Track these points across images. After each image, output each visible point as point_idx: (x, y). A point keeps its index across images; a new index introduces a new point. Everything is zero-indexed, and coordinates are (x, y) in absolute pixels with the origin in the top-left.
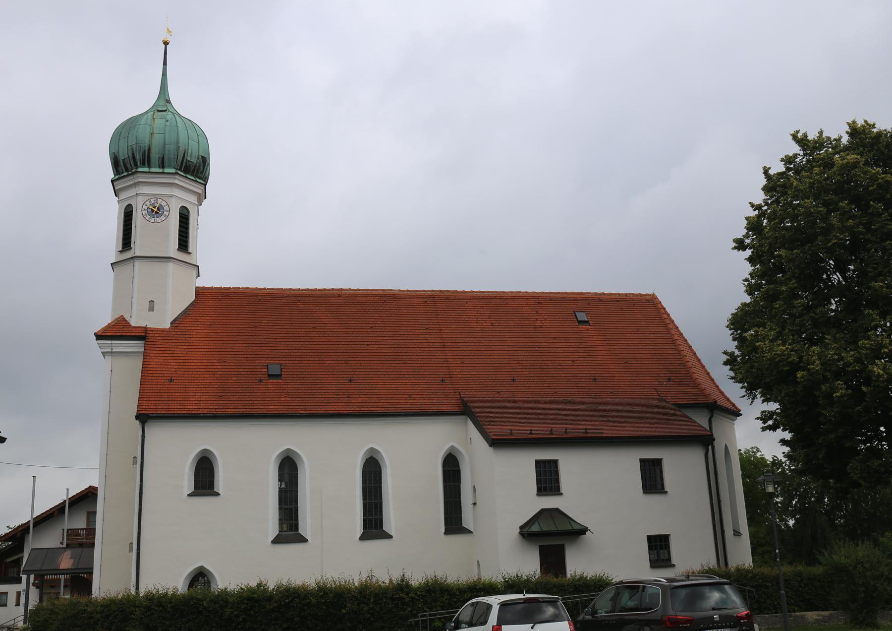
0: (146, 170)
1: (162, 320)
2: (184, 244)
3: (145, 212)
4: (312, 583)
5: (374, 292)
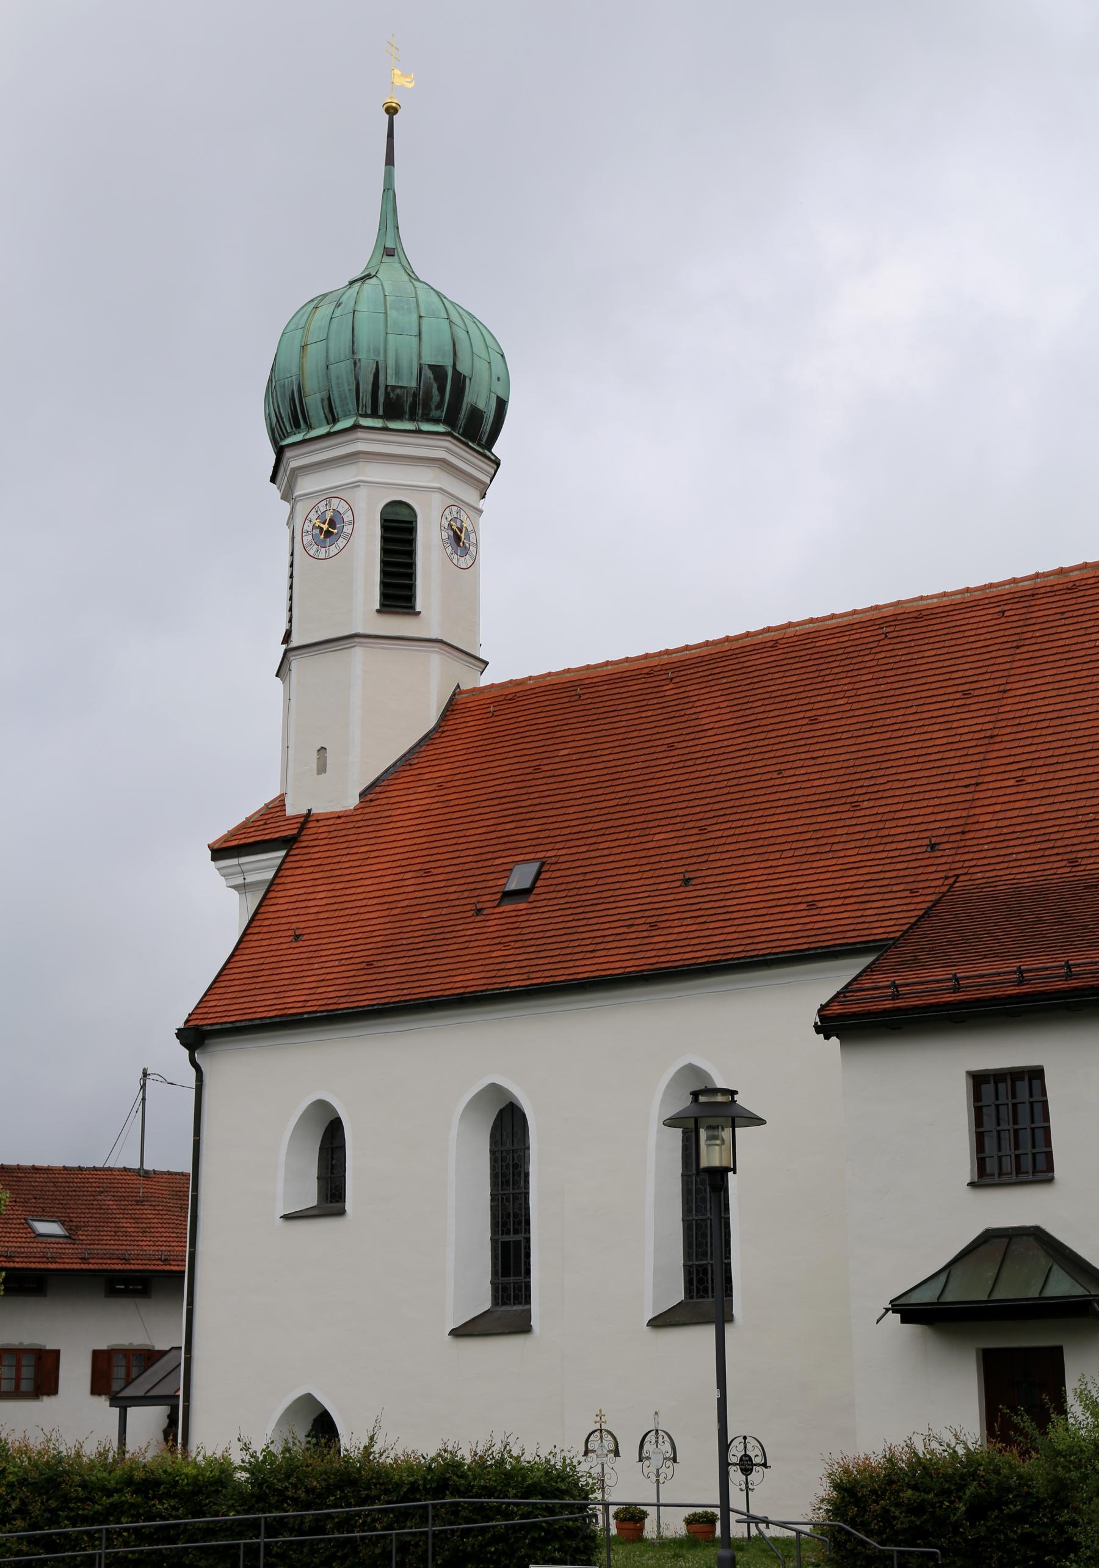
0: (298, 437)
1: (338, 794)
2: (398, 591)
3: (308, 538)
4: (877, 1459)
5: (876, 615)
